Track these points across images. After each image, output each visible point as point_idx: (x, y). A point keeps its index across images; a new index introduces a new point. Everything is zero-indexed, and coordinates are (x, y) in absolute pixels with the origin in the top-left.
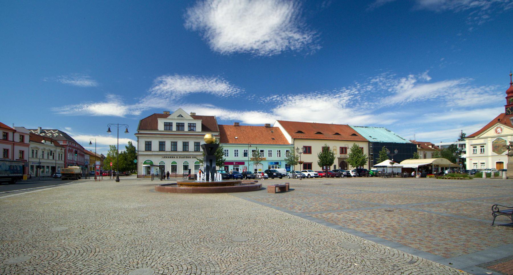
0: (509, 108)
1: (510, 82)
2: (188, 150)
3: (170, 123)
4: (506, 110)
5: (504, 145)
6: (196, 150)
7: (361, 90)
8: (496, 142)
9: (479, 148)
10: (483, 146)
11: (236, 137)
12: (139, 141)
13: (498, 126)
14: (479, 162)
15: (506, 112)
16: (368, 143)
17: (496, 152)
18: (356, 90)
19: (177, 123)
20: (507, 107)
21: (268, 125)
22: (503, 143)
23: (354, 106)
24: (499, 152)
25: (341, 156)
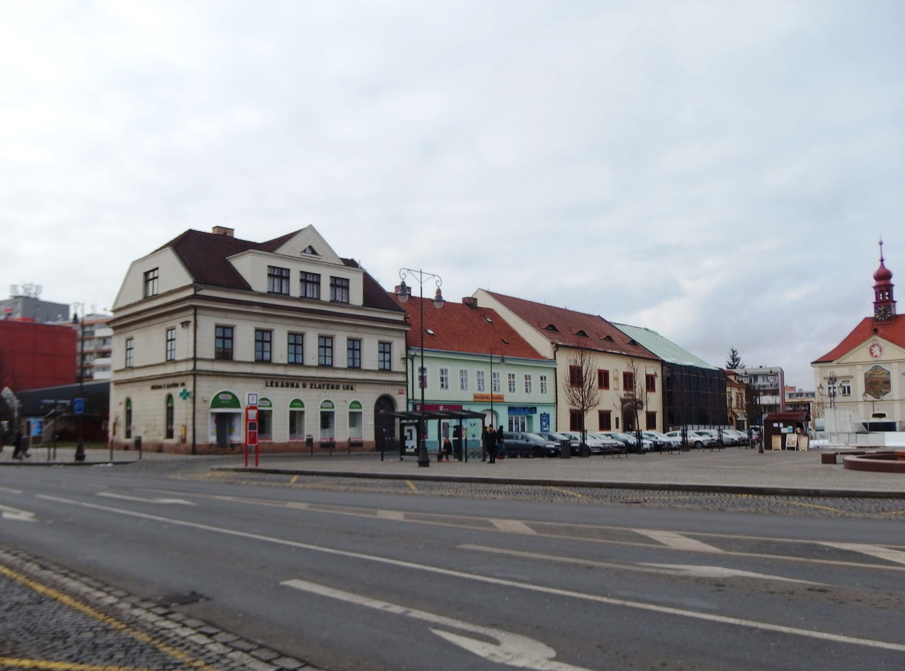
1: (880, 258)
3: (282, 269)
4: (875, 312)
5: (887, 379)
6: (292, 360)
8: (871, 374)
11: (430, 332)
12: (199, 323)
17: (872, 393)
22: (884, 376)
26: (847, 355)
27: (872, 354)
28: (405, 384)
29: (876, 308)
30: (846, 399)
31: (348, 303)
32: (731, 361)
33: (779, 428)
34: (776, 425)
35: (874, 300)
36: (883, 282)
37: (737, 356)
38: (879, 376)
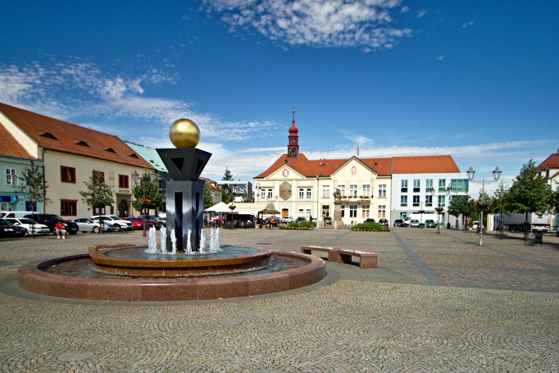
0: (291, 148)
1: (292, 120)
4: (288, 151)
7: (47, 80)
8: (282, 186)
9: (305, 191)
10: (271, 190)
13: (286, 168)
14: (305, 207)
15: (288, 153)
16: (154, 171)
18: (37, 77)
20: (289, 147)
22: (289, 187)
23: (32, 103)
24: (285, 197)
25: (120, 191)
27: (284, 175)
30: (308, 199)
38: (286, 187)
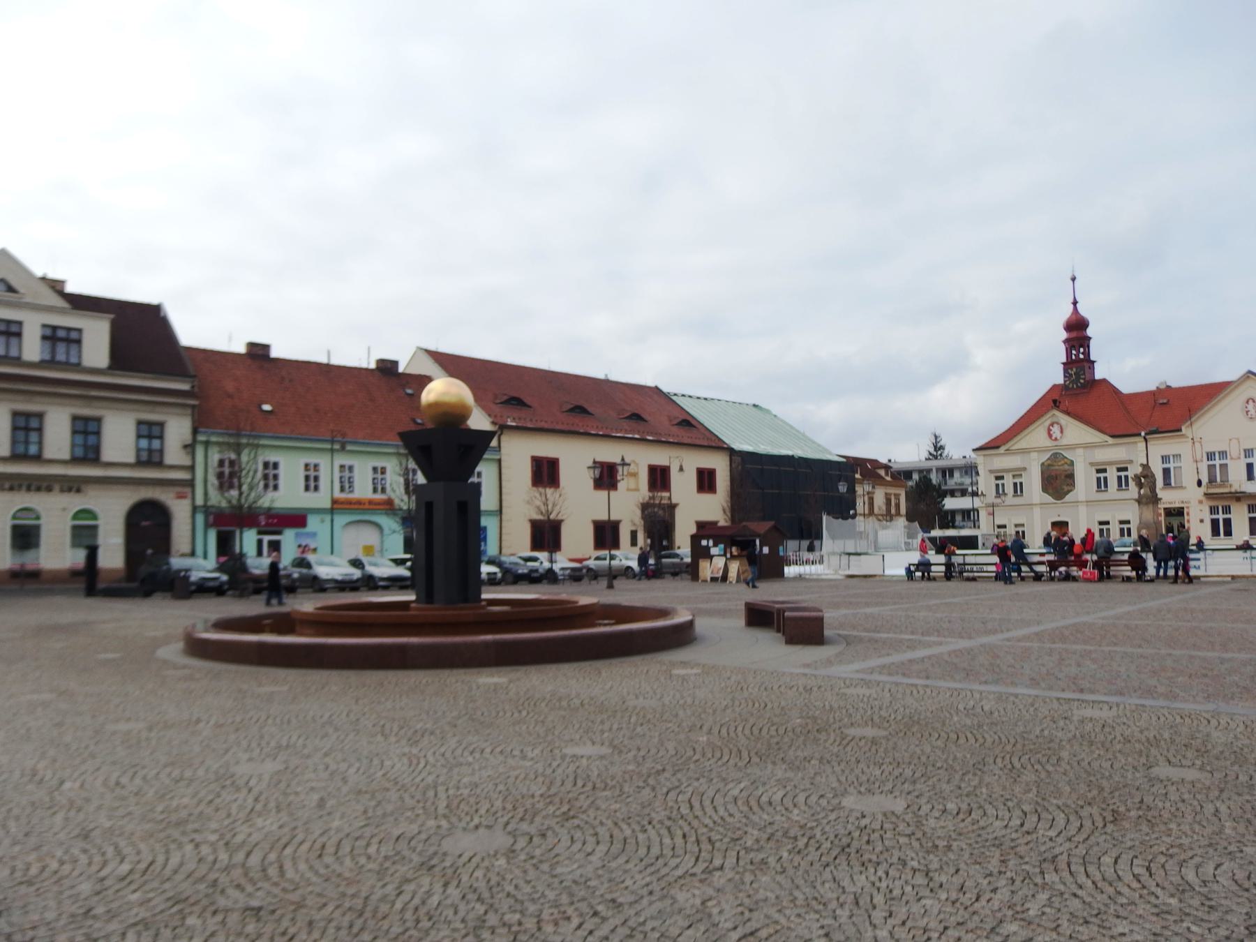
2: (33, 449)
4: (1065, 376)
8: (1049, 465)
11: (267, 407)
17: (1051, 491)
19: (44, 326)
21: (389, 365)
22: (1066, 467)
26: (1019, 437)
27: (1050, 436)
28: (191, 483)
29: (1065, 371)
30: (1018, 501)
31: (79, 364)
32: (932, 450)
33: (708, 548)
34: (704, 543)
35: (1064, 360)
36: (1074, 334)
37: (942, 443)
38: (1060, 467)
